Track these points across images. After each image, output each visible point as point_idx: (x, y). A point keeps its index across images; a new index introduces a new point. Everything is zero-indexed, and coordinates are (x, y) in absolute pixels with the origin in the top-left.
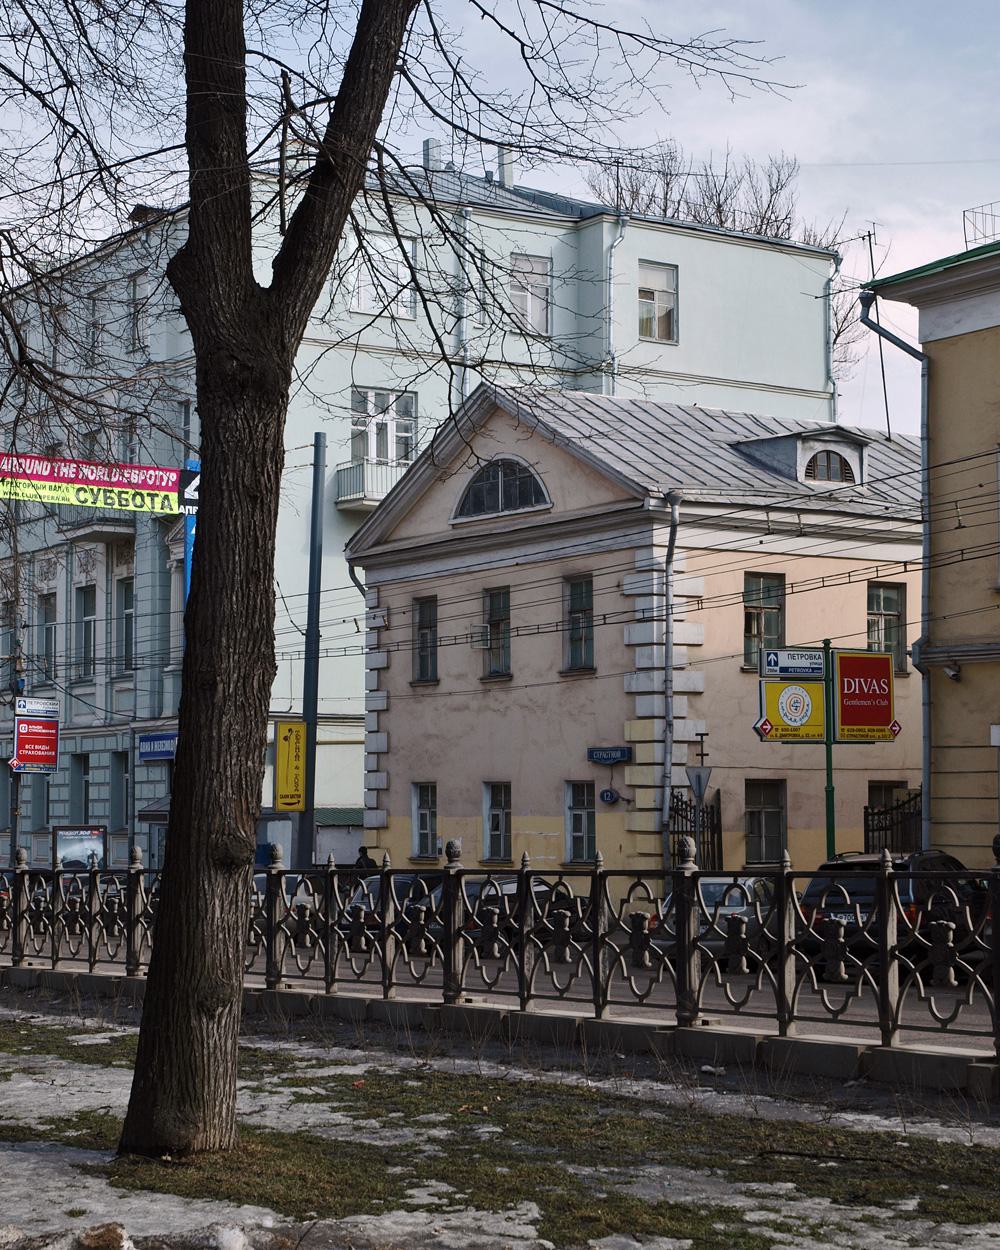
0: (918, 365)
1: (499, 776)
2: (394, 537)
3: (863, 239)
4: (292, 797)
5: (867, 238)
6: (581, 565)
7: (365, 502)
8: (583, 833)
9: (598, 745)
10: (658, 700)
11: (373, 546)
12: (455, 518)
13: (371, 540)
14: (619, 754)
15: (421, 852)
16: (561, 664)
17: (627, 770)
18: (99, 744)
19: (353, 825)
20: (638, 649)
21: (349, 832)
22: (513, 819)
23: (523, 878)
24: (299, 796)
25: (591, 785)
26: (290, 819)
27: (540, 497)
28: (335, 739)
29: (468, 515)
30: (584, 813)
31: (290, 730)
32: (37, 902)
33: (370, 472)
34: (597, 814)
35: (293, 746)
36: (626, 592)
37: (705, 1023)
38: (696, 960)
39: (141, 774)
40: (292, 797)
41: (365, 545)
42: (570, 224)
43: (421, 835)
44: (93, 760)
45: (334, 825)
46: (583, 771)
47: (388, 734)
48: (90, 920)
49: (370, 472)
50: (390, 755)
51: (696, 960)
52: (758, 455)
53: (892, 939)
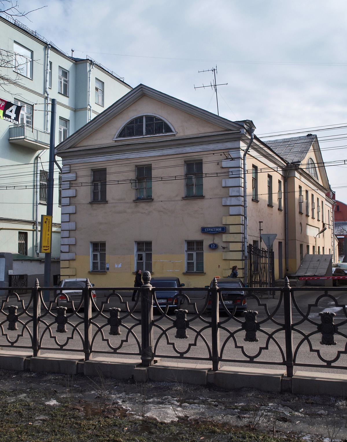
1: (145, 238)
2: (79, 145)
3: (213, 71)
4: (47, 247)
5: (214, 71)
7: (25, 140)
9: (206, 226)
10: (242, 208)
11: (68, 148)
12: (116, 138)
13: (68, 146)
14: (220, 229)
15: (188, 270)
16: (183, 194)
17: (224, 236)
19: (24, 260)
20: (230, 189)
21: (22, 262)
22: (107, 256)
24: (49, 247)
25: (200, 243)
26: (4, 257)
28: (7, 228)
29: (124, 136)
30: (144, 254)
31: (47, 219)
33: (26, 131)
34: (204, 253)
35: (47, 226)
37: (156, 362)
40: (47, 247)
41: (65, 148)
42: (74, 62)
43: (188, 263)
45: (18, 260)
46: (197, 236)
47: (76, 223)
49: (26, 131)
50: (76, 231)
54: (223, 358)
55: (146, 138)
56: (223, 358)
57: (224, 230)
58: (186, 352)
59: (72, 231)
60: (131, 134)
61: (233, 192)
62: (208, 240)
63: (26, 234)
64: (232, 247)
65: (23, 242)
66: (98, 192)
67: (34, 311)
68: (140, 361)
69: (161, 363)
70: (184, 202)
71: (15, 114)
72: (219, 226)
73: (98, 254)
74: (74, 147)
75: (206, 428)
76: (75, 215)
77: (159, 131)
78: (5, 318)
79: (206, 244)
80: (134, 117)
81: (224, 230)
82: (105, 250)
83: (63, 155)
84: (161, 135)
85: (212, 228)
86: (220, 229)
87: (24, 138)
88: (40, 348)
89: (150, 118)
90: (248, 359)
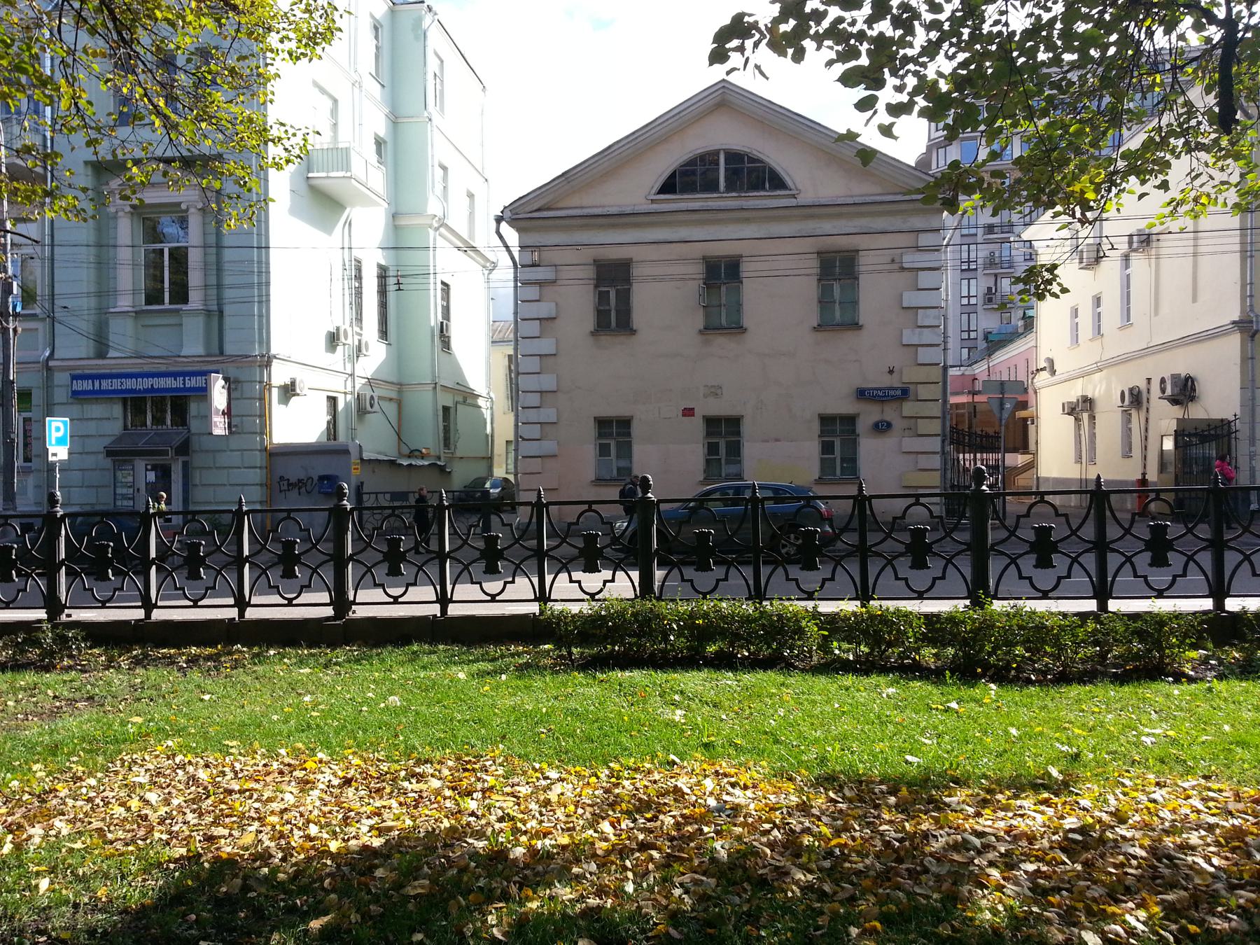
2: (560, 205)
13: (536, 206)
14: (899, 393)
25: (849, 421)
36: (905, 265)
46: (845, 407)
54: (529, 508)
55: (723, 200)
56: (529, 508)
59: (549, 394)
60: (690, 188)
62: (869, 415)
64: (924, 427)
66: (610, 311)
70: (820, 335)
71: (849, 130)
72: (896, 385)
73: (613, 444)
74: (549, 209)
75: (937, 820)
76: (552, 360)
77: (757, 185)
79: (863, 425)
80: (699, 151)
83: (523, 224)
84: (762, 193)
85: (880, 389)
86: (899, 393)
87: (351, 177)
89: (735, 158)
90: (489, 598)
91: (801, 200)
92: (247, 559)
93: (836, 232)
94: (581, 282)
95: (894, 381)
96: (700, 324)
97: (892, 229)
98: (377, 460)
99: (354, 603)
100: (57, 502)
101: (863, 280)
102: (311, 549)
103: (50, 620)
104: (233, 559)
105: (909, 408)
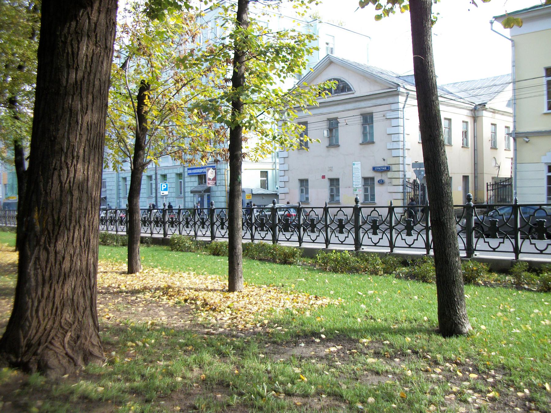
0: (510, 42)
6: (368, 110)
8: (369, 193)
18: (171, 171)
23: (515, 207)
25: (372, 179)
27: (350, 89)
32: (172, 218)
36: (388, 117)
37: (476, 255)
38: (254, 227)
39: (187, 179)
44: (168, 176)
46: (370, 174)
48: (116, 221)
51: (254, 227)
52: (406, 80)
53: (253, 221)
57: (388, 169)
58: (378, 242)
61: (394, 138)
62: (378, 177)
63: (267, 172)
64: (395, 182)
65: (265, 179)
67: (19, 231)
68: (465, 255)
69: (366, 249)
70: (361, 146)
78: (370, 227)
81: (388, 169)
82: (308, 185)
85: (379, 167)
88: (395, 247)
90: (539, 252)
91: (357, 94)
92: (519, 230)
93: (366, 106)
94: (525, 96)
95: (385, 164)
96: (327, 144)
97: (382, 103)
98: (268, 194)
99: (475, 250)
100: (471, 199)
101: (375, 124)
102: (504, 225)
103: (355, 250)
104: (512, 229)
105: (390, 174)
